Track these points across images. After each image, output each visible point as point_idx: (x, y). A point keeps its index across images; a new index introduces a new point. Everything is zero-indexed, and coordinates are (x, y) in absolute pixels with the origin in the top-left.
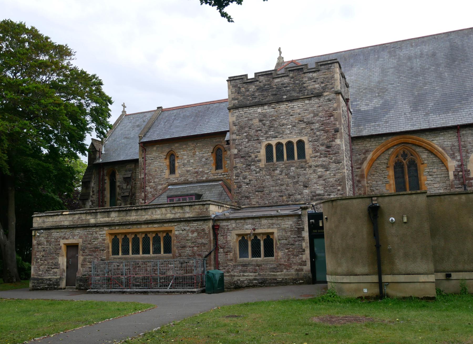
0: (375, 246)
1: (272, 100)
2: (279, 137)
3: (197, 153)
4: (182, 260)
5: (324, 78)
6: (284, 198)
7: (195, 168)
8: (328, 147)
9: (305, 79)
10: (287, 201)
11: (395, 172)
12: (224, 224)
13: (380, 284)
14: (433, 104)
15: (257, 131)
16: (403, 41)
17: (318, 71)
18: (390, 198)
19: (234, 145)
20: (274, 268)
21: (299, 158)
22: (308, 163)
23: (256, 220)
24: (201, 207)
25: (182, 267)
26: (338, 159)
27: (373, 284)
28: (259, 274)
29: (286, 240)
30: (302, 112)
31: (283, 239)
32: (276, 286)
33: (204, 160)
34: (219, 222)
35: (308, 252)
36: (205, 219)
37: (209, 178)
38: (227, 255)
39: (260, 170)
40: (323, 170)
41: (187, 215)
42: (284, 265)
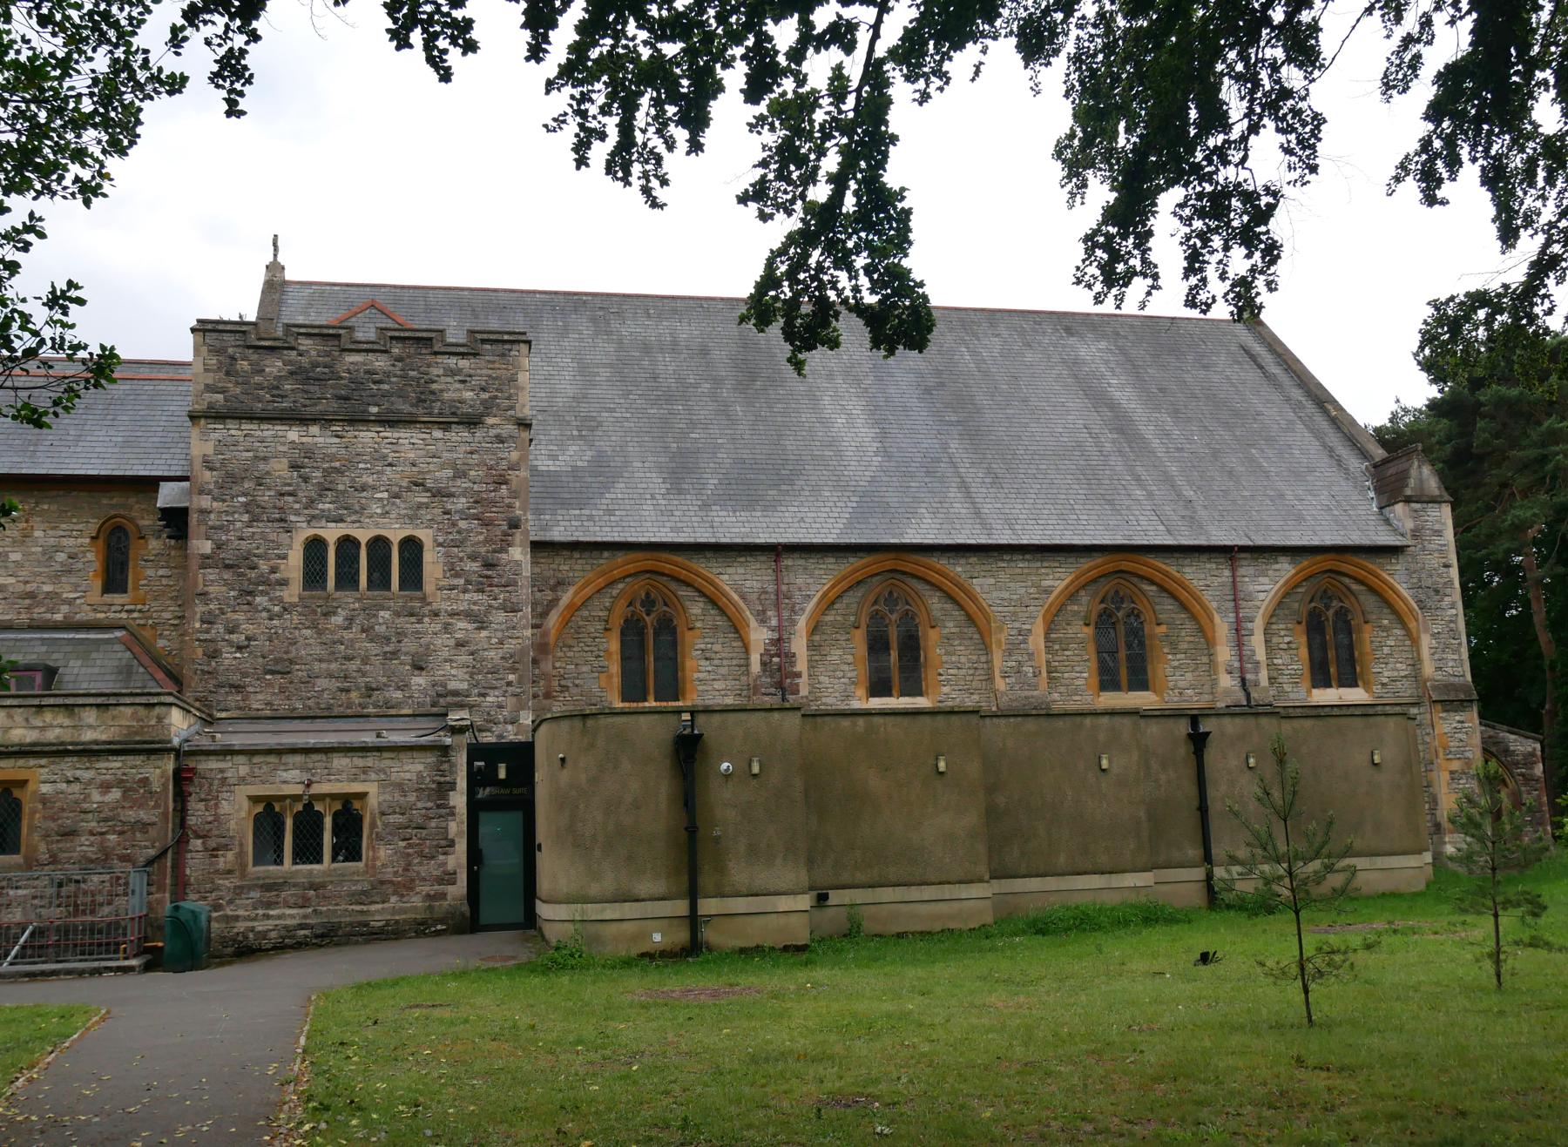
0: (686, 829)
1: (335, 413)
2: (349, 519)
3: (38, 534)
4: (59, 875)
5: (490, 376)
6: (354, 695)
7: (27, 582)
8: (489, 565)
9: (435, 371)
10: (360, 705)
11: (624, 644)
12: (213, 764)
13: (694, 920)
14: (716, 482)
15: (282, 495)
16: (624, 296)
17: (475, 355)
18: (725, 715)
19: (203, 528)
20: (364, 893)
21: (403, 585)
22: (429, 604)
23: (315, 757)
24: (142, 711)
25: (59, 896)
26: (514, 600)
27: (676, 922)
28: (315, 911)
29: (403, 814)
30: (422, 460)
31: (395, 813)
32: (367, 942)
33: (61, 557)
34: (192, 758)
35: (462, 847)
36: (153, 749)
37: (78, 616)
38: (216, 856)
39: (285, 609)
40: (470, 627)
41: (88, 736)
42: (391, 882)
